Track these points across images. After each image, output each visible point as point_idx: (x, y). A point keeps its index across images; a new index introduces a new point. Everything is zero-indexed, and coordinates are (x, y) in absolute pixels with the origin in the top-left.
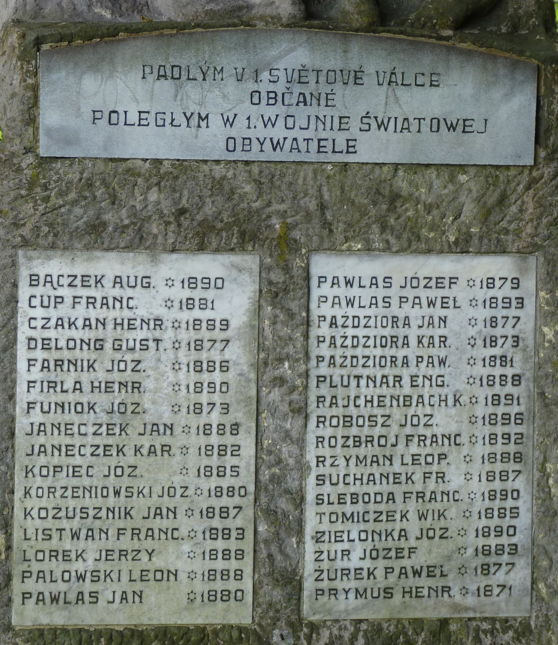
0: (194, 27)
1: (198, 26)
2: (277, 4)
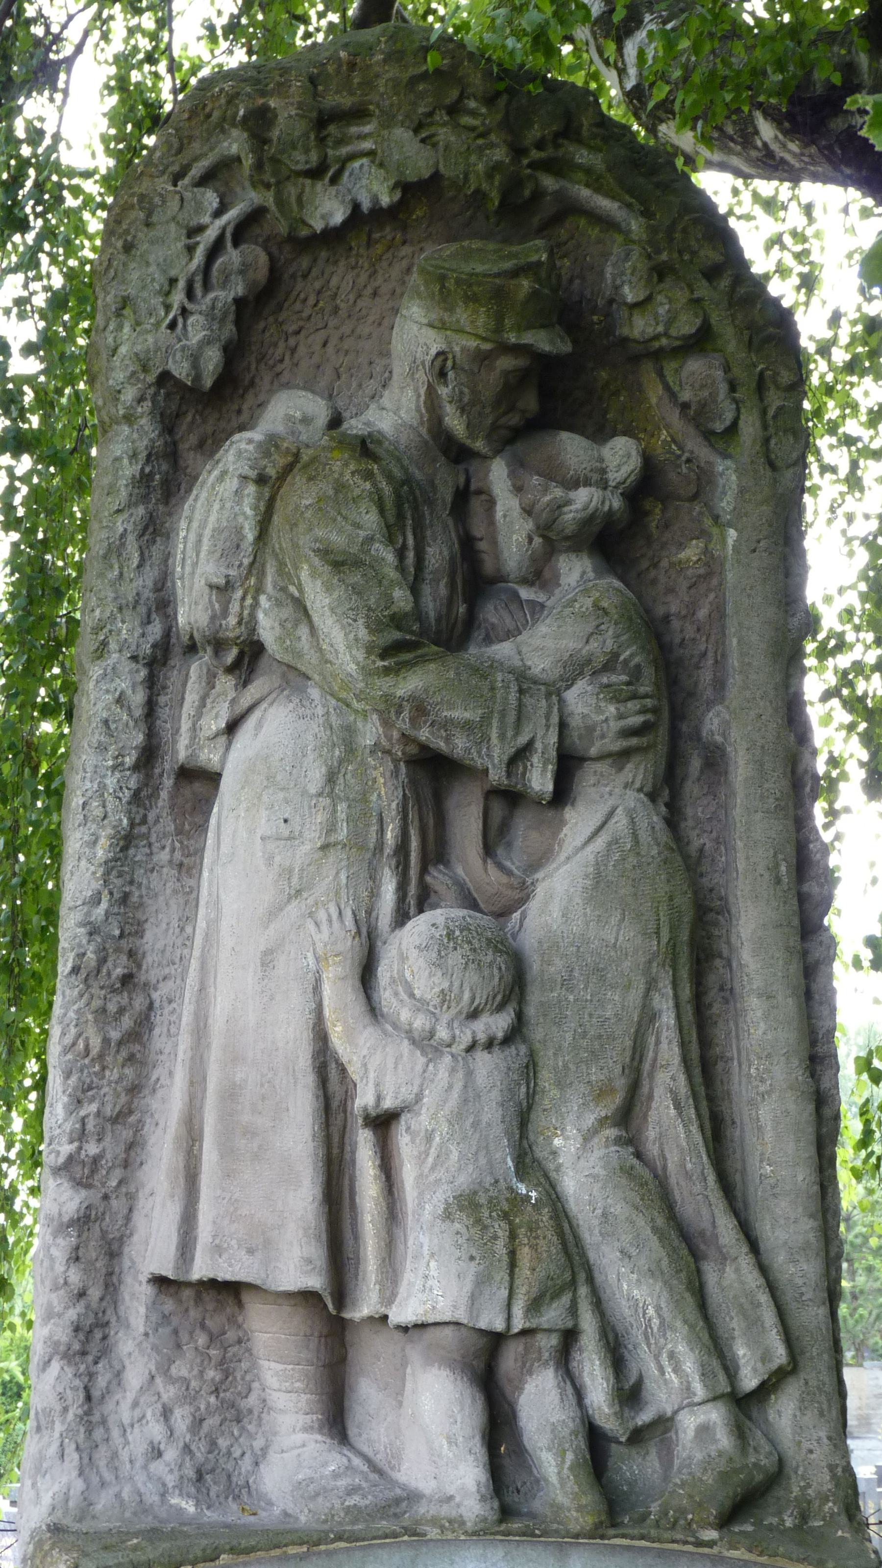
0: (333, 1541)
1: (339, 1538)
2: (458, 1499)
